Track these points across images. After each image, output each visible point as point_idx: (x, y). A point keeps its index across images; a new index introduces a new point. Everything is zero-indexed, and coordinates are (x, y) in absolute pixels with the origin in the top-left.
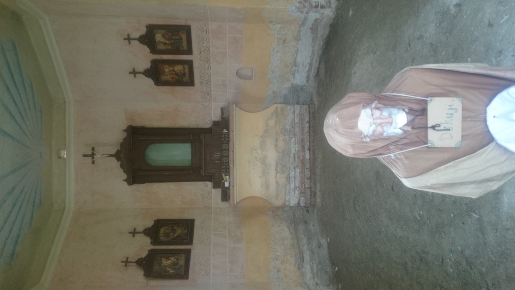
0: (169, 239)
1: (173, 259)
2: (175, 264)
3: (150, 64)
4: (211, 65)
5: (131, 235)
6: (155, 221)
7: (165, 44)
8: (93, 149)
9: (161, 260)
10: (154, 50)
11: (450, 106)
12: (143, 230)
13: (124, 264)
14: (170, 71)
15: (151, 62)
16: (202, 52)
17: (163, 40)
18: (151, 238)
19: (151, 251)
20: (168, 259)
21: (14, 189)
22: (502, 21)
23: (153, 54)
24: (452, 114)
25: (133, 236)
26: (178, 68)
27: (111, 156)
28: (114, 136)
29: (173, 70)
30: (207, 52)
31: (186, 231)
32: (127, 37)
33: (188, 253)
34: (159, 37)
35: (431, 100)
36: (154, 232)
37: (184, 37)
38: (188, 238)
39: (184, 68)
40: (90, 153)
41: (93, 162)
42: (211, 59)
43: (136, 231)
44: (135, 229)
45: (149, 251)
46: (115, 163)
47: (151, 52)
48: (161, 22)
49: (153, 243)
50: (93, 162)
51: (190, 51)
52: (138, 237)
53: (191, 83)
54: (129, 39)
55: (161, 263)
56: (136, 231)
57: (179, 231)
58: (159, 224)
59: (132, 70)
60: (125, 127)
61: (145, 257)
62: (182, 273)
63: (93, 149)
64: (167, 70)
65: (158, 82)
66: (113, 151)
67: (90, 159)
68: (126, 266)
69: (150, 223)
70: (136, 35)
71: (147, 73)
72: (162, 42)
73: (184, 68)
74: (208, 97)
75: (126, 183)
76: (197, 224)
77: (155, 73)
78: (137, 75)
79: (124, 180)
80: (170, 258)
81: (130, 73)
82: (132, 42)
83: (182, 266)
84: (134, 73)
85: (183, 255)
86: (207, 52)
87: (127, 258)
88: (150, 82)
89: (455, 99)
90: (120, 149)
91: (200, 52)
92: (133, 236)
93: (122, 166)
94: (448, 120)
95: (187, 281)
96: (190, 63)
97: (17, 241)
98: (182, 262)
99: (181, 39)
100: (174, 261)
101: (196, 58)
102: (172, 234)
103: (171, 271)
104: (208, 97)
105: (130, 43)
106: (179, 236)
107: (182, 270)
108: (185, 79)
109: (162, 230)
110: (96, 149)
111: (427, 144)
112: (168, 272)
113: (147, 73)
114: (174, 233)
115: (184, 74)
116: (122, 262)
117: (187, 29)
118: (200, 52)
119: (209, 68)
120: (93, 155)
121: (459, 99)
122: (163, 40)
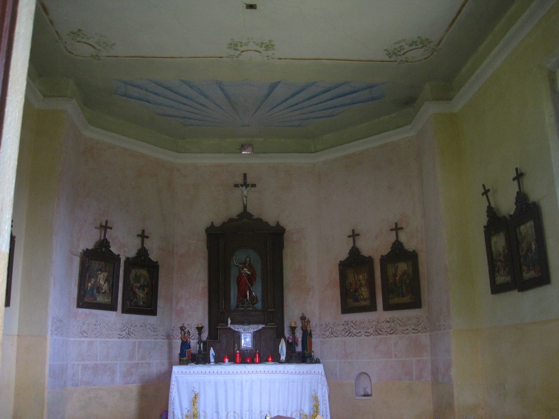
0: (132, 282)
2: (99, 289)
3: (368, 256)
4: (372, 337)
5: (140, 233)
6: (157, 262)
7: (395, 275)
8: (254, 186)
9: (106, 271)
10: (385, 260)
12: (146, 248)
13: (104, 224)
14: (360, 280)
15: (370, 257)
16: (388, 324)
17: (399, 273)
18: (135, 258)
19: (118, 258)
20: (107, 280)
21: (206, 97)
22: (212, 352)
23: (381, 260)
25: (138, 236)
26: (364, 292)
27: (245, 207)
28: (269, 211)
29: (361, 285)
30: (389, 330)
31: (141, 303)
32: (399, 226)
33: (112, 307)
34: (403, 267)
36: (142, 261)
37: (406, 299)
38: (130, 308)
39: (365, 300)
40: (249, 181)
41: (236, 186)
42: (379, 336)
43: (145, 239)
44: (147, 237)
45: (119, 255)
46: (235, 210)
48: (423, 269)
49: (128, 259)
50: (236, 186)
51: (388, 307)
52: (138, 241)
53: (346, 309)
54: (397, 229)
55: (102, 272)
56: (145, 239)
57: (141, 294)
58: (153, 268)
59: (357, 233)
60: (283, 223)
61: (111, 251)
63: (254, 186)
64: (361, 277)
66: (250, 209)
67: (240, 181)
68: (101, 226)
69: (153, 257)
70: (403, 238)
71: (355, 252)
72: (396, 271)
73: (365, 300)
74: (371, 331)
75: (209, 225)
76: (150, 319)
77: (354, 264)
78: (351, 239)
79: (212, 222)
80: (107, 283)
81: (353, 231)
82: (394, 232)
83: (96, 299)
84: (354, 235)
85: (110, 300)
86: (389, 330)
87: (111, 228)
88: (344, 255)
90: (253, 217)
91: (388, 322)
92: (138, 236)
93: (231, 220)
96: (372, 308)
97: (143, 100)
98: (100, 299)
99: (403, 296)
100: (102, 289)
101: (380, 315)
102: (139, 285)
103: (90, 284)
104: (327, 333)
105: (391, 230)
106: (135, 294)
107: (90, 299)
109: (144, 272)
110: (253, 189)
112: (89, 281)
113: (355, 252)
114: (139, 289)
115: (357, 300)
116: (107, 222)
117: (416, 304)
118: (388, 322)
119: (368, 334)
120: (246, 185)
122: (399, 273)
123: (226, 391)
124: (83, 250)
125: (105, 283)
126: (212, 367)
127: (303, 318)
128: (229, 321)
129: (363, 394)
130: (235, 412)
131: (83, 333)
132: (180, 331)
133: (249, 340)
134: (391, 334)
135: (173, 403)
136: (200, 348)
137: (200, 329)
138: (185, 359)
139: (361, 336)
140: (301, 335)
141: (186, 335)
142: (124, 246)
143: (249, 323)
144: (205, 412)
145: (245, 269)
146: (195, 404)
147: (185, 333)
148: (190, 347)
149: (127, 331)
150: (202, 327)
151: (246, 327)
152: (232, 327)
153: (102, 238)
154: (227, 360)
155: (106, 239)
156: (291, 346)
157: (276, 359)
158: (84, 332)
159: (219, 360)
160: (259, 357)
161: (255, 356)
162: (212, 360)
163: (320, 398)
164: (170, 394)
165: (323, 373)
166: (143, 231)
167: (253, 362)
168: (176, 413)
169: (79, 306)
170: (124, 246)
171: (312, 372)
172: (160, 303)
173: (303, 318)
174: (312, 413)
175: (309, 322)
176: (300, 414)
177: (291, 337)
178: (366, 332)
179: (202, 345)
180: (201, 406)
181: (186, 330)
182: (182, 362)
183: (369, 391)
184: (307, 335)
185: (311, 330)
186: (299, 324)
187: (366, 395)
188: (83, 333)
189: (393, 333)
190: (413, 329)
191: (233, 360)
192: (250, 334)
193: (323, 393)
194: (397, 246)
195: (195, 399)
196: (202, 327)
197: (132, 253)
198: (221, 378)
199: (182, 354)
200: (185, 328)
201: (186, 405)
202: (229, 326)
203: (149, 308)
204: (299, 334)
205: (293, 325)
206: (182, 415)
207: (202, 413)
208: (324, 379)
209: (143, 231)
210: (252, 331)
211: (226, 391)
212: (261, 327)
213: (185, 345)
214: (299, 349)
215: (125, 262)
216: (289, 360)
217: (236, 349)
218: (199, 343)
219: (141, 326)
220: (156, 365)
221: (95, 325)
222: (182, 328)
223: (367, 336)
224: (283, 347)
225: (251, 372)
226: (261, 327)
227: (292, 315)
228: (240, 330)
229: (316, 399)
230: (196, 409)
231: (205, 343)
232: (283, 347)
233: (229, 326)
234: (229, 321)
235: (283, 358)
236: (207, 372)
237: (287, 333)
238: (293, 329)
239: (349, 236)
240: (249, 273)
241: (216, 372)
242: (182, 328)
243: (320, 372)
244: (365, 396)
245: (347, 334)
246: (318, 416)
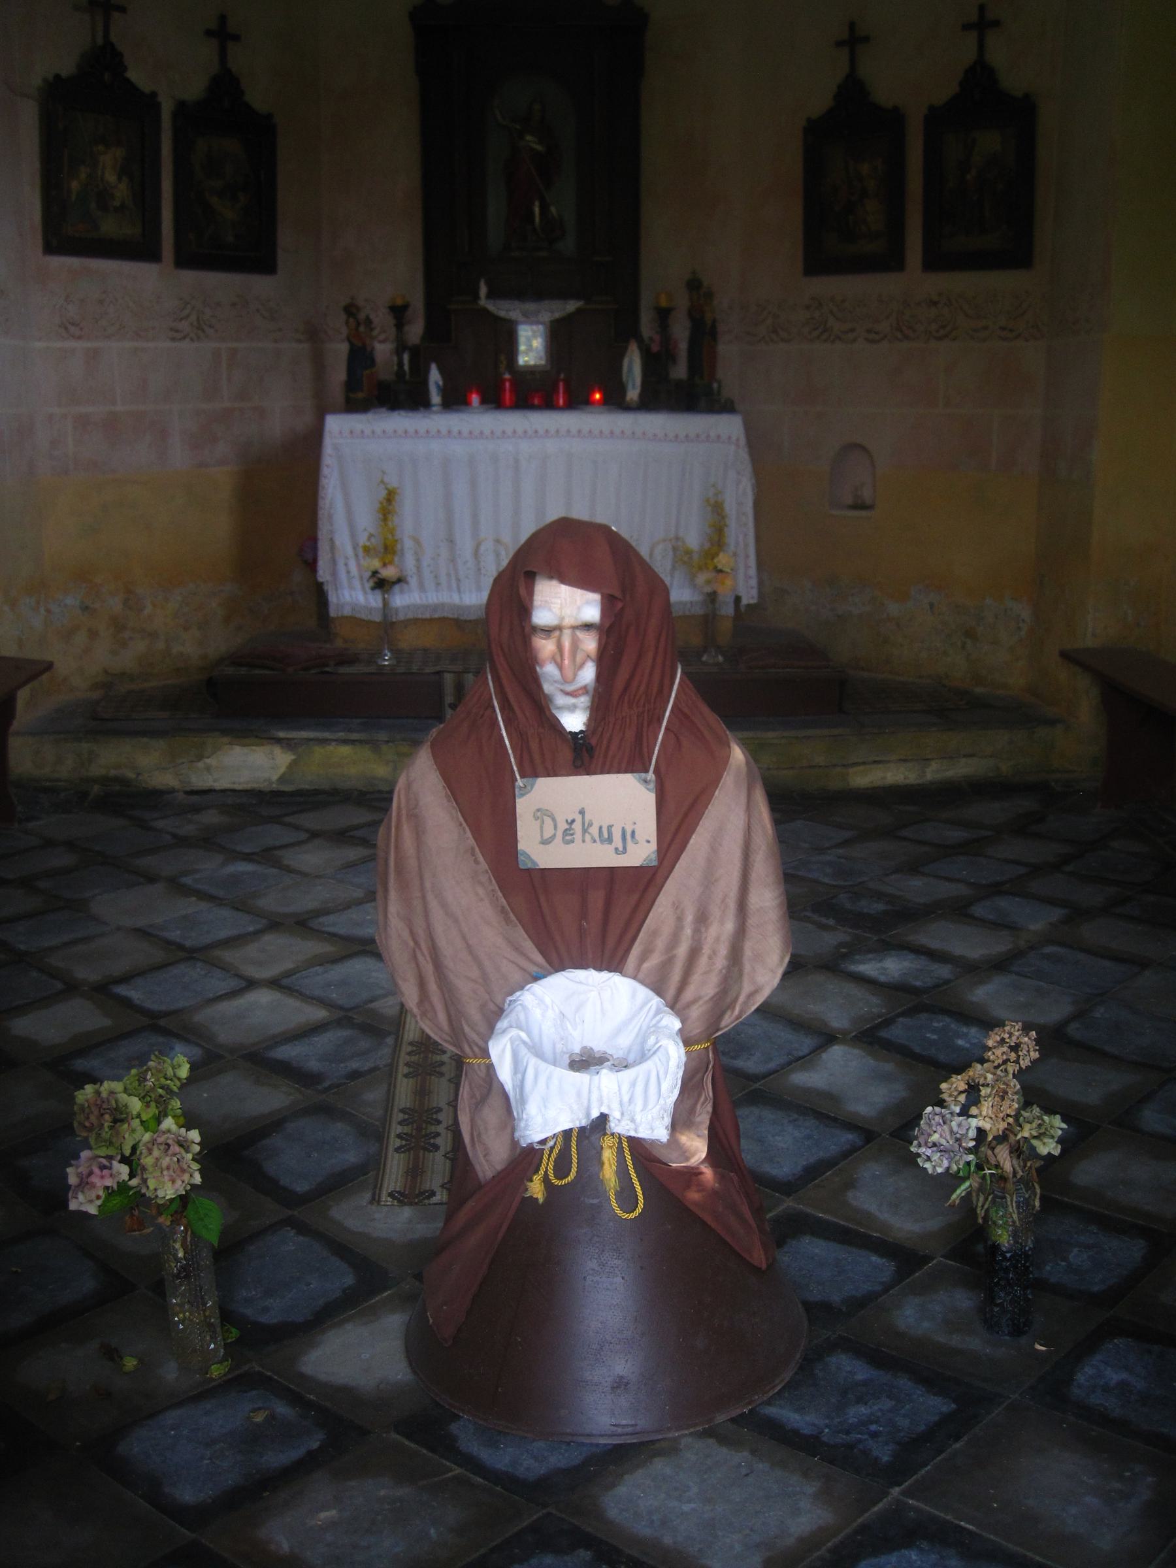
1: (122, 191)
10: (937, 119)
11: (633, 833)
15: (896, 109)
19: (151, 102)
22: (435, 376)
24: (610, 840)
25: (209, 33)
33: (143, 250)
34: (989, 142)
35: (645, 781)
36: (223, 110)
44: (236, 38)
45: (154, 95)
47: (932, 108)
49: (181, 109)
51: (935, 261)
53: (818, 261)
54: (983, 24)
58: (259, 133)
61: (128, 81)
62: (67, 231)
65: (821, 136)
69: (258, 96)
70: (999, 54)
76: (260, 285)
77: (850, 125)
81: (852, 26)
84: (854, 40)
88: (819, 101)
89: (653, 846)
91: (935, 304)
92: (209, 33)
94: (594, 830)
95: (40, 250)
96: (892, 261)
98: (110, 227)
101: (914, 282)
108: (835, 239)
111: (522, 776)
113: (852, 91)
117: (1017, 255)
118: (935, 304)
121: (654, 856)
123: (473, 484)
124: (45, 80)
125: (120, 179)
126: (436, 417)
127: (694, 285)
128: (483, 290)
129: (849, 500)
130: (498, 541)
131: (70, 327)
132: (343, 317)
133: (538, 343)
134: (939, 339)
135: (330, 517)
136: (400, 364)
137: (399, 312)
138: (360, 395)
139: (854, 340)
140: (687, 334)
141: (362, 329)
142: (168, 66)
143: (539, 295)
144: (417, 541)
145: (529, 138)
146: (390, 517)
147: (359, 324)
148: (373, 362)
149: (193, 318)
150: (405, 307)
151: (531, 306)
152: (491, 306)
153: (100, 41)
154: (475, 399)
155: (112, 45)
156: (655, 364)
157: (616, 401)
158: (73, 324)
159: (454, 400)
160: (568, 391)
161: (555, 390)
162: (436, 398)
163: (730, 507)
164: (321, 493)
165: (743, 441)
166: (223, 19)
167: (548, 405)
168: (337, 543)
169: (50, 248)
170: (168, 66)
171: (713, 434)
172: (286, 238)
173: (694, 285)
174: (707, 546)
175: (710, 295)
176: (675, 549)
177: (657, 338)
178: (869, 331)
179: (406, 357)
180: (406, 523)
181: (362, 316)
182: (354, 405)
183: (867, 494)
184: (704, 334)
185: (714, 321)
186: (682, 302)
187: (860, 506)
188: (70, 327)
189: (946, 336)
190: (1003, 329)
191: (494, 400)
192: (541, 327)
193: (739, 496)
194: (979, 80)
195: (388, 505)
196: (405, 307)
197: (194, 89)
198: (458, 449)
199: (352, 384)
200: (358, 309)
201: (366, 520)
202: (483, 302)
203: (253, 253)
204: (681, 331)
205: (664, 303)
206: (355, 548)
207: (408, 544)
208: (744, 454)
209: (223, 19)
210: (547, 317)
211: (473, 484)
212: (572, 306)
213: (360, 357)
214: (680, 371)
215: (175, 115)
216: (650, 402)
217: (502, 367)
218: (399, 351)
219: (234, 305)
220: (279, 414)
221: (101, 302)
222: (351, 310)
223: (873, 341)
224: (633, 367)
225: (541, 432)
226: (572, 306)
227: (663, 270)
228: (514, 315)
229: (716, 508)
230: (392, 532)
231: (415, 352)
232: (633, 367)
233: (483, 302)
234: (483, 290)
235: (633, 394)
236: (422, 431)
237: (647, 326)
238: (663, 315)
239: (839, 44)
240: (539, 148)
241: (444, 431)
242: (351, 310)
243: (734, 439)
244: (855, 507)
245: (816, 333)
246: (721, 555)
